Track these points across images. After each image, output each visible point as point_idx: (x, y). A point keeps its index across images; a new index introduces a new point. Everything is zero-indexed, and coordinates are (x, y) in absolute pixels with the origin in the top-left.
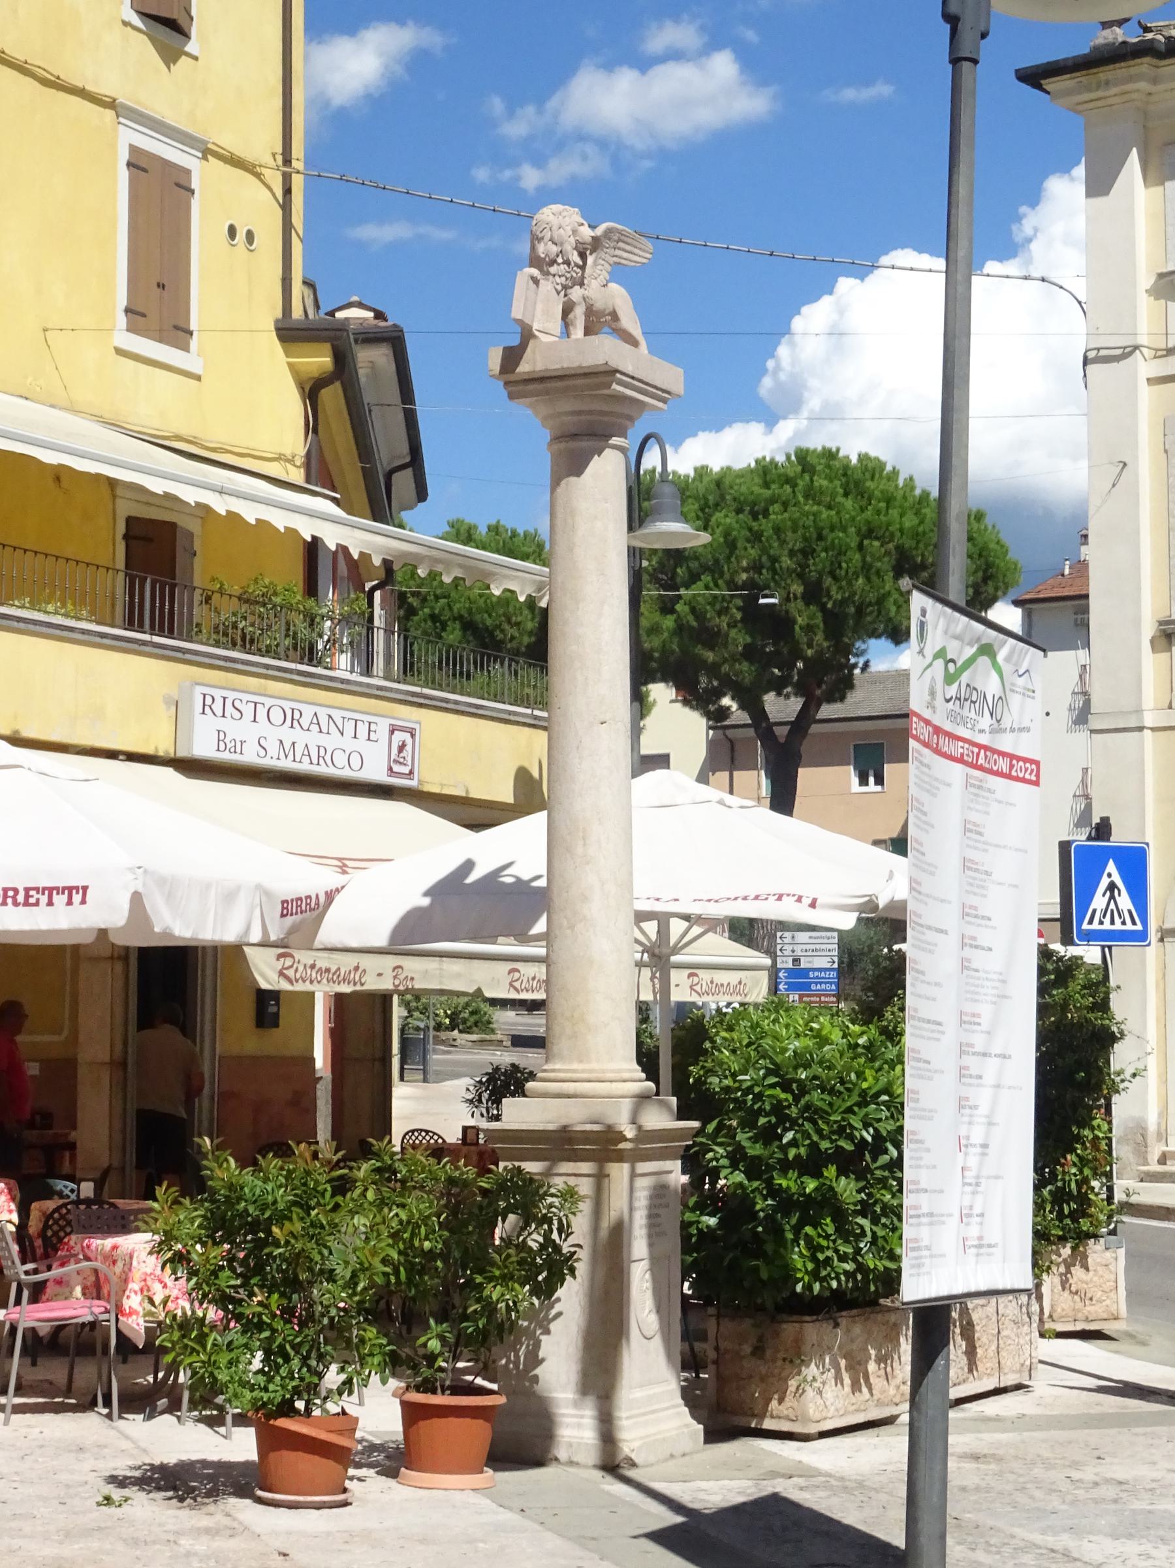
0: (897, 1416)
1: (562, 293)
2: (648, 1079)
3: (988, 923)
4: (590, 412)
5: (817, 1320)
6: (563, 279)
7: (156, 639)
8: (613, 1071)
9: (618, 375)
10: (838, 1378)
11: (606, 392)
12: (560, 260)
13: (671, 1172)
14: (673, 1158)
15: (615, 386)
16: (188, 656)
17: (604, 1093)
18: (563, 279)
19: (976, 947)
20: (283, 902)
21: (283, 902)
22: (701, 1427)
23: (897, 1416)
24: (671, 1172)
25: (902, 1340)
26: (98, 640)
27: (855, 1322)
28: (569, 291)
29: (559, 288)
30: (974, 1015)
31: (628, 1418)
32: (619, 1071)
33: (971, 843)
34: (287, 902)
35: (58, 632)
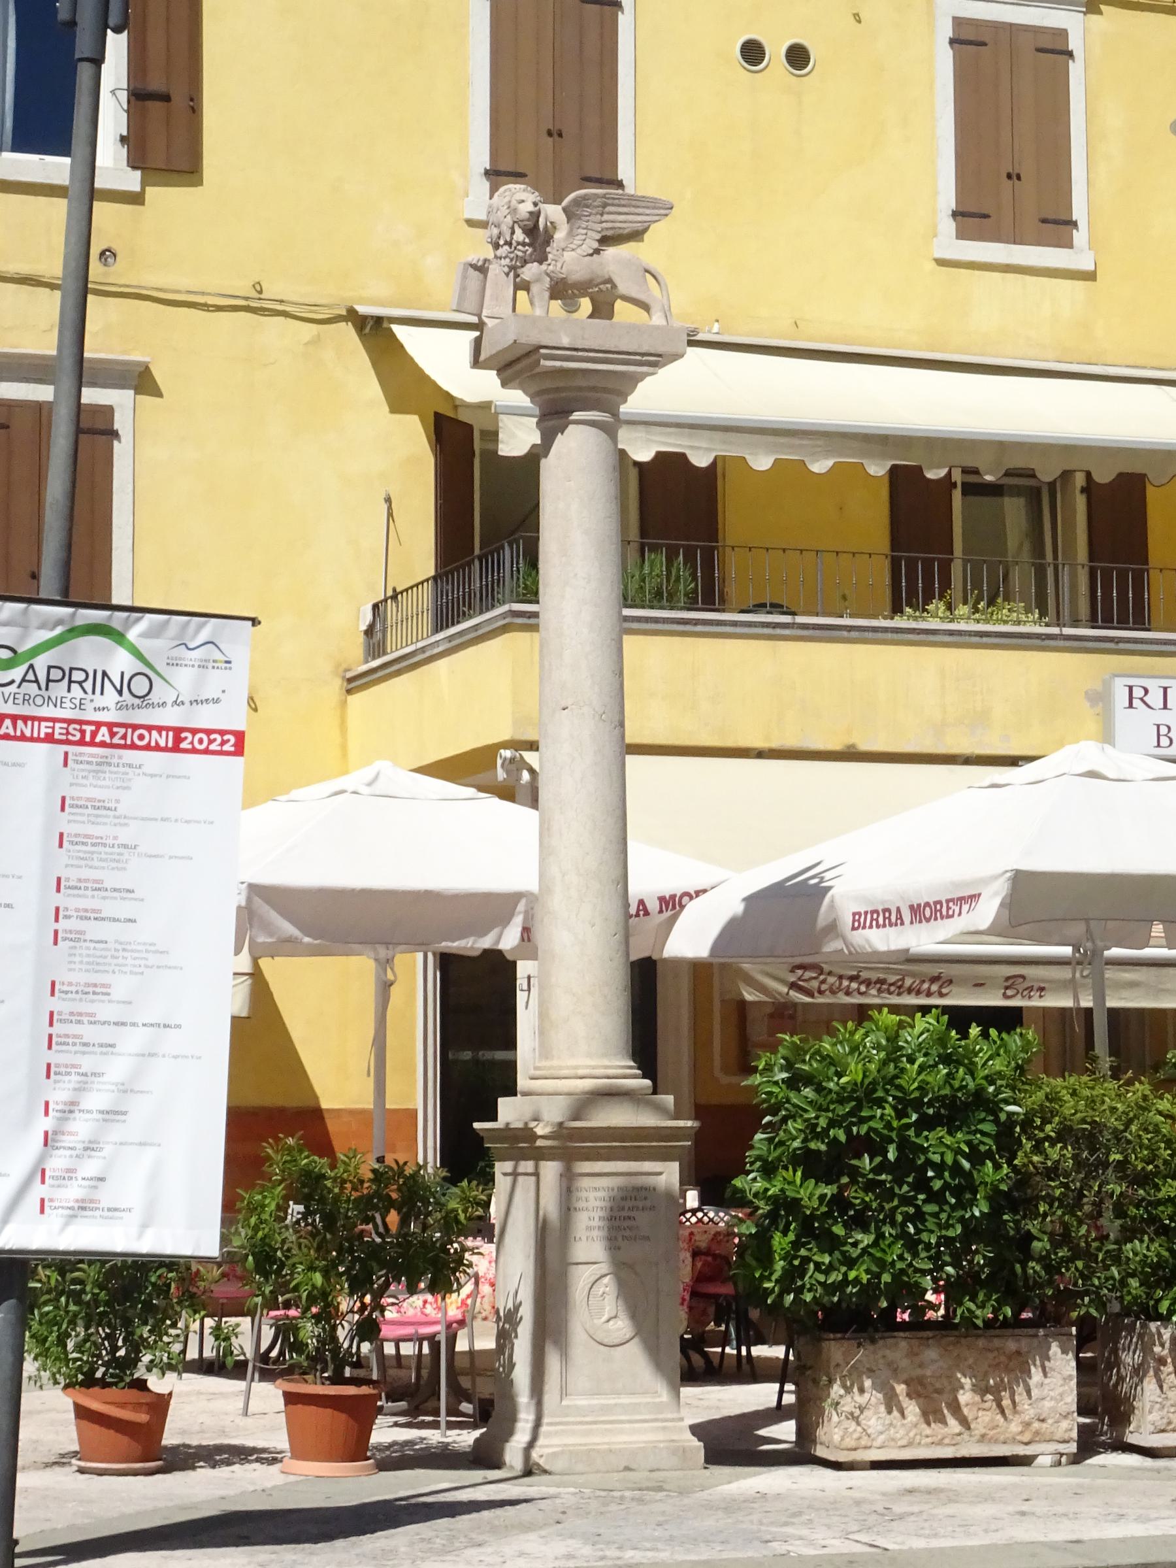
0: (1035, 1457)
1: (512, 274)
2: (644, 1077)
3: (132, 895)
4: (557, 390)
5: (843, 1338)
6: (508, 260)
7: (1067, 631)
8: (568, 1068)
9: (542, 351)
10: (891, 1403)
11: (538, 370)
12: (501, 242)
13: (660, 1174)
14: (664, 1156)
15: (543, 362)
16: (1122, 646)
17: (550, 1090)
18: (508, 260)
19: (103, 919)
20: (854, 914)
21: (854, 914)
22: (701, 1444)
23: (1035, 1457)
24: (660, 1174)
25: (1033, 1369)
26: (947, 639)
27: (928, 1346)
28: (519, 271)
29: (506, 269)
30: (103, 986)
31: (551, 1424)
32: (576, 1067)
33: (72, 818)
34: (859, 914)
35: (911, 637)
